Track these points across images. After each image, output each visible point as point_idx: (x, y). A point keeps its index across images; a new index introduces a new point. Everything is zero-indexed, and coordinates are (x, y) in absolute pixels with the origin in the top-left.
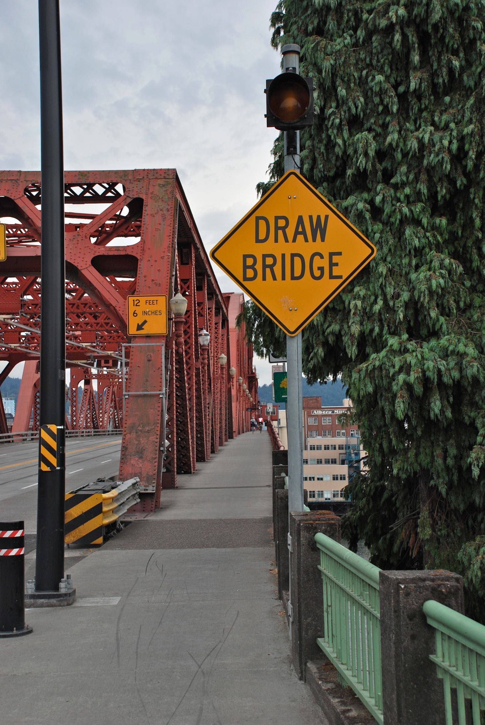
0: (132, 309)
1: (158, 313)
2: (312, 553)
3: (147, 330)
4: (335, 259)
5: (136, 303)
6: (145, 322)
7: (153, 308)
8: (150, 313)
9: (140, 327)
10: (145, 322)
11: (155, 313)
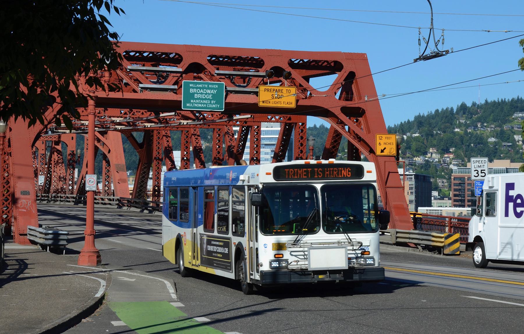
0: (378, 141)
1: (391, 144)
2: (420, 120)
3: (386, 153)
4: (477, 175)
5: (380, 138)
6: (385, 148)
7: (389, 141)
8: (387, 144)
9: (382, 151)
10: (385, 148)
11: (390, 144)
